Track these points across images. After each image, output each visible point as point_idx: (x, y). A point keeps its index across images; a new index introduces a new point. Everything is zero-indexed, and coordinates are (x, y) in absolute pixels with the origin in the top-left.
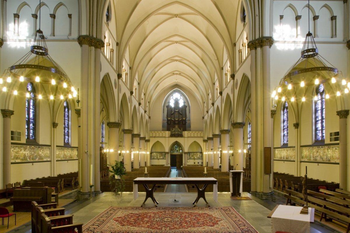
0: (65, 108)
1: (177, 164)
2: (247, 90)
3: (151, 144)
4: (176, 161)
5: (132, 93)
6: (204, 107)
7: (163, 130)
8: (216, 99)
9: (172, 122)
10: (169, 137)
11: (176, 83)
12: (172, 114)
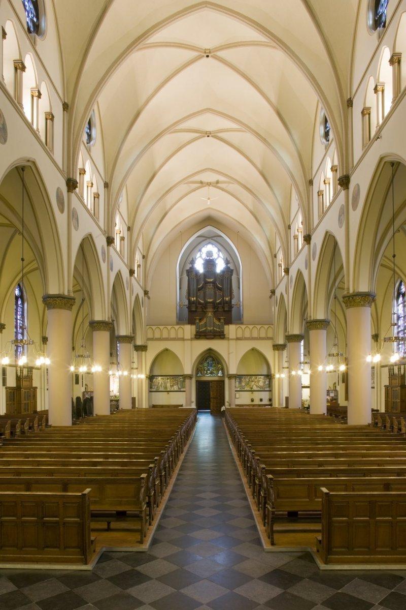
0: (17, 298)
1: (211, 404)
2: (332, 262)
3: (150, 355)
4: (209, 396)
5: (132, 272)
6: (273, 267)
7: (178, 324)
8: (293, 259)
9: (201, 306)
10: (192, 339)
11: (205, 214)
12: (199, 290)
